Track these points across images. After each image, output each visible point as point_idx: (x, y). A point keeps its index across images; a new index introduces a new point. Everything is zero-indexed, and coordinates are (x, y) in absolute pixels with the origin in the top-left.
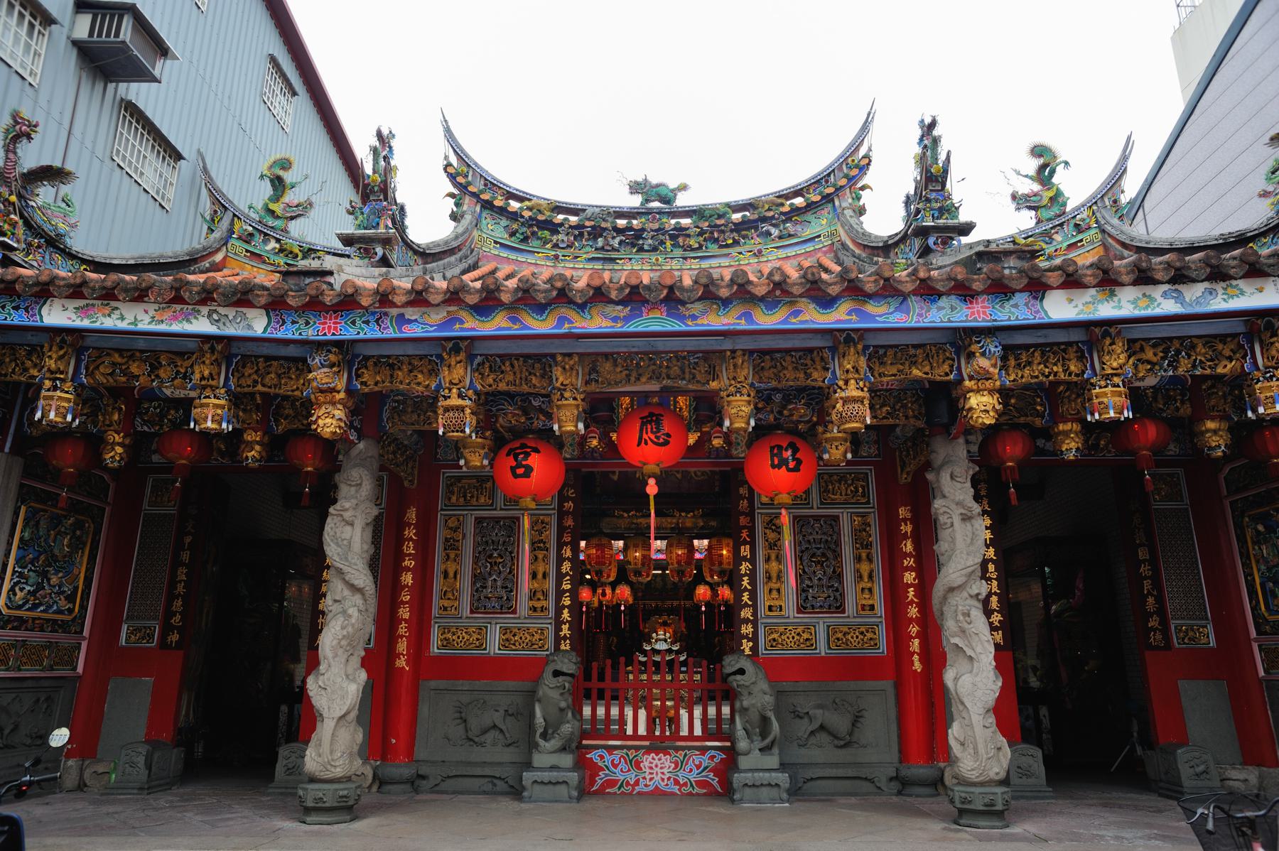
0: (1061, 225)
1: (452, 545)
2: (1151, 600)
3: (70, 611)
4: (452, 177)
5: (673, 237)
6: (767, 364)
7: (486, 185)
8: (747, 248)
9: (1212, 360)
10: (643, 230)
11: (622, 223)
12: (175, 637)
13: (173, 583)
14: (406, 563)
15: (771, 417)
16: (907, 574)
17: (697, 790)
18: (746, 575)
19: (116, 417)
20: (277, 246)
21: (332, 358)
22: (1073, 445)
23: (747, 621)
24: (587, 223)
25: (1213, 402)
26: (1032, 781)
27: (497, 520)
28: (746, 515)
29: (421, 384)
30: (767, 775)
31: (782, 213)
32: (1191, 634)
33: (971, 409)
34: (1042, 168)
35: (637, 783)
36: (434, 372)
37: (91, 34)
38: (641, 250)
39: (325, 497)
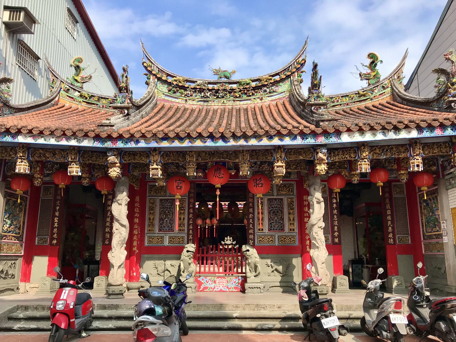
0: (378, 86)
1: (152, 209)
2: (390, 228)
3: (19, 233)
4: (146, 68)
5: (230, 93)
6: (254, 154)
7: (159, 71)
8: (257, 97)
9: (398, 153)
10: (218, 90)
11: (210, 87)
12: (55, 242)
13: (53, 223)
14: (136, 215)
15: (257, 169)
16: (305, 219)
17: (234, 290)
18: (251, 218)
19: (38, 169)
20: (79, 94)
21: (115, 153)
22: (356, 179)
23: (251, 234)
24: (198, 87)
25: (403, 165)
26: (344, 287)
27: (167, 200)
28: (252, 198)
29: (144, 160)
30: (256, 284)
31: (271, 83)
32: (403, 239)
33: (317, 169)
34: (373, 62)
35: (215, 288)
36: (148, 157)
37: (10, 19)
38: (218, 97)
39: (112, 196)
